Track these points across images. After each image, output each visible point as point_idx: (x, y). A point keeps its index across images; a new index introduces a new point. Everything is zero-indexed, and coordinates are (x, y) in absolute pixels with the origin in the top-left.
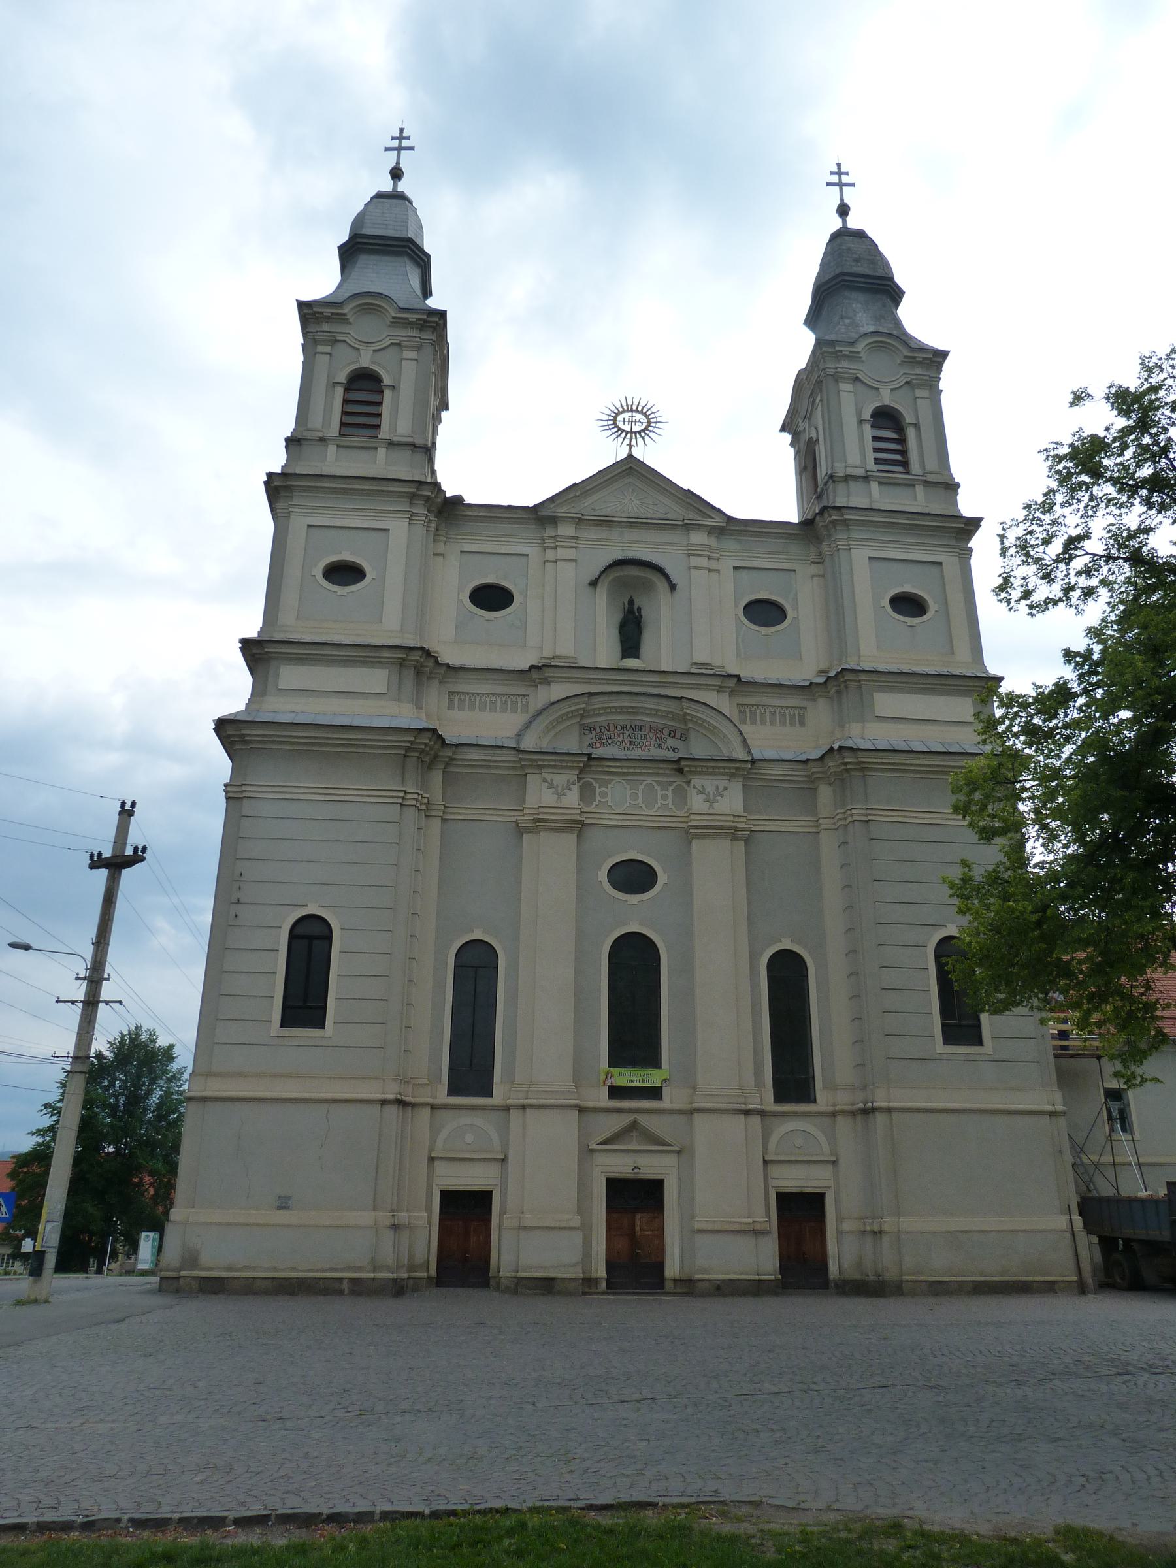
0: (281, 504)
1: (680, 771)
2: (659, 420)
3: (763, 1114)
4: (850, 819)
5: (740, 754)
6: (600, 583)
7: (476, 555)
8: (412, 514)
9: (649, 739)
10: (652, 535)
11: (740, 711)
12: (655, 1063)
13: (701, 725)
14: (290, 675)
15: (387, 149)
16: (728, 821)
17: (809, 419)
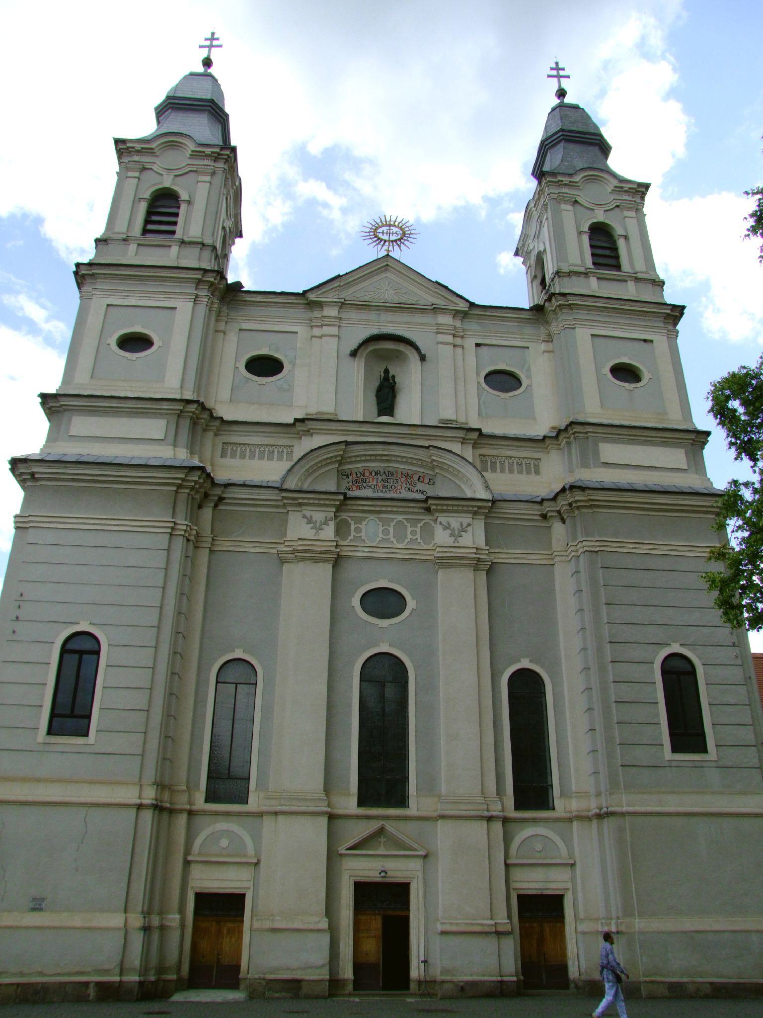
0: (86, 288)
1: (428, 510)
2: (412, 232)
3: (505, 820)
4: (581, 550)
5: (482, 494)
6: (359, 354)
8: (197, 296)
9: (400, 484)
10: (406, 317)
11: (482, 462)
13: (447, 471)
14: (81, 425)
15: (201, 47)
16: (471, 553)
17: (538, 238)
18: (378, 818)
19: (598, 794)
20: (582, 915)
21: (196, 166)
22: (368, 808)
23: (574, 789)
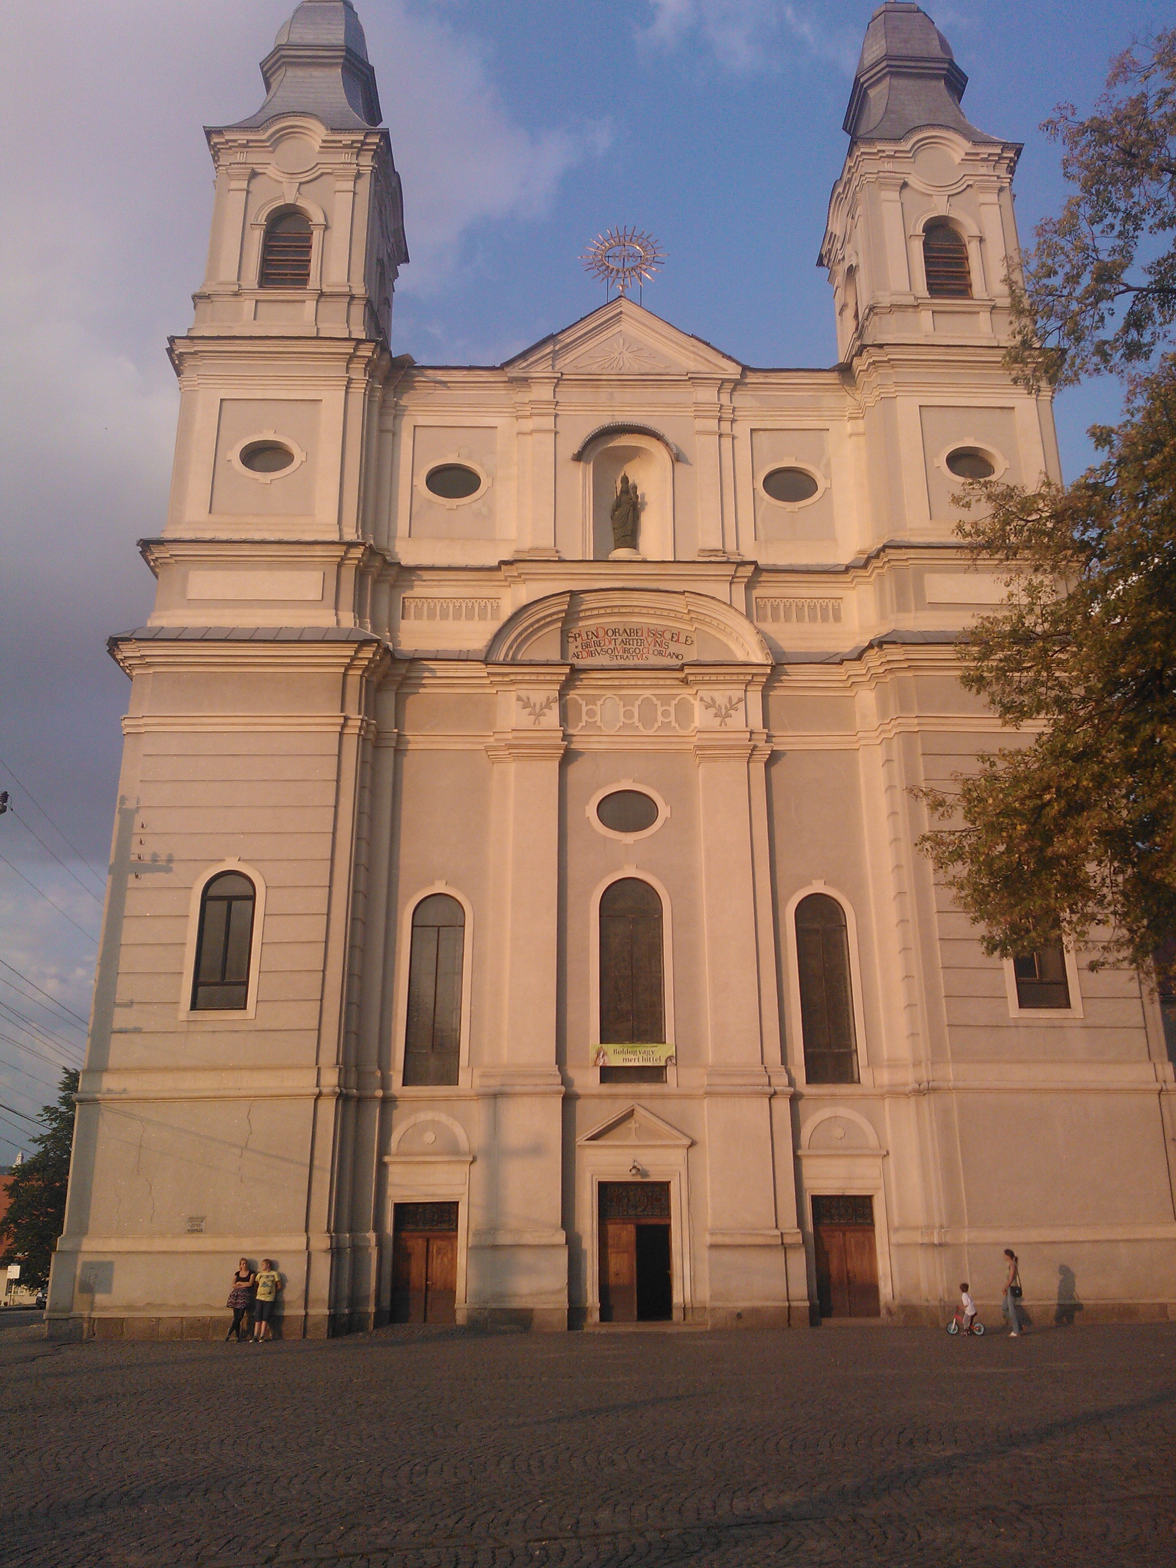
5: (758, 656)
7: (431, 428)
10: (649, 394)
12: (656, 1035)
13: (709, 624)
18: (626, 1096)
19: (916, 1064)
20: (896, 1222)
21: (330, 166)
22: (613, 1085)
23: (885, 1055)
